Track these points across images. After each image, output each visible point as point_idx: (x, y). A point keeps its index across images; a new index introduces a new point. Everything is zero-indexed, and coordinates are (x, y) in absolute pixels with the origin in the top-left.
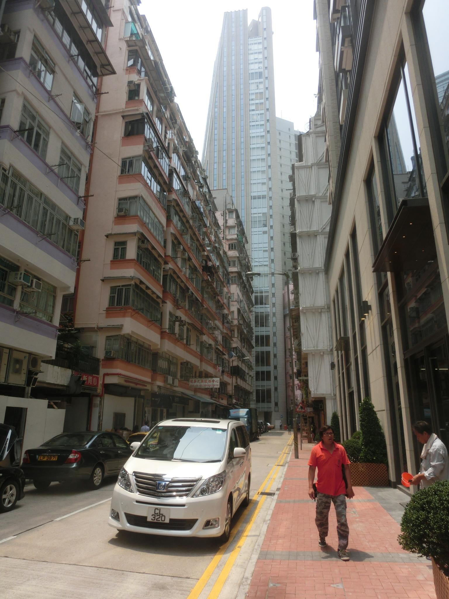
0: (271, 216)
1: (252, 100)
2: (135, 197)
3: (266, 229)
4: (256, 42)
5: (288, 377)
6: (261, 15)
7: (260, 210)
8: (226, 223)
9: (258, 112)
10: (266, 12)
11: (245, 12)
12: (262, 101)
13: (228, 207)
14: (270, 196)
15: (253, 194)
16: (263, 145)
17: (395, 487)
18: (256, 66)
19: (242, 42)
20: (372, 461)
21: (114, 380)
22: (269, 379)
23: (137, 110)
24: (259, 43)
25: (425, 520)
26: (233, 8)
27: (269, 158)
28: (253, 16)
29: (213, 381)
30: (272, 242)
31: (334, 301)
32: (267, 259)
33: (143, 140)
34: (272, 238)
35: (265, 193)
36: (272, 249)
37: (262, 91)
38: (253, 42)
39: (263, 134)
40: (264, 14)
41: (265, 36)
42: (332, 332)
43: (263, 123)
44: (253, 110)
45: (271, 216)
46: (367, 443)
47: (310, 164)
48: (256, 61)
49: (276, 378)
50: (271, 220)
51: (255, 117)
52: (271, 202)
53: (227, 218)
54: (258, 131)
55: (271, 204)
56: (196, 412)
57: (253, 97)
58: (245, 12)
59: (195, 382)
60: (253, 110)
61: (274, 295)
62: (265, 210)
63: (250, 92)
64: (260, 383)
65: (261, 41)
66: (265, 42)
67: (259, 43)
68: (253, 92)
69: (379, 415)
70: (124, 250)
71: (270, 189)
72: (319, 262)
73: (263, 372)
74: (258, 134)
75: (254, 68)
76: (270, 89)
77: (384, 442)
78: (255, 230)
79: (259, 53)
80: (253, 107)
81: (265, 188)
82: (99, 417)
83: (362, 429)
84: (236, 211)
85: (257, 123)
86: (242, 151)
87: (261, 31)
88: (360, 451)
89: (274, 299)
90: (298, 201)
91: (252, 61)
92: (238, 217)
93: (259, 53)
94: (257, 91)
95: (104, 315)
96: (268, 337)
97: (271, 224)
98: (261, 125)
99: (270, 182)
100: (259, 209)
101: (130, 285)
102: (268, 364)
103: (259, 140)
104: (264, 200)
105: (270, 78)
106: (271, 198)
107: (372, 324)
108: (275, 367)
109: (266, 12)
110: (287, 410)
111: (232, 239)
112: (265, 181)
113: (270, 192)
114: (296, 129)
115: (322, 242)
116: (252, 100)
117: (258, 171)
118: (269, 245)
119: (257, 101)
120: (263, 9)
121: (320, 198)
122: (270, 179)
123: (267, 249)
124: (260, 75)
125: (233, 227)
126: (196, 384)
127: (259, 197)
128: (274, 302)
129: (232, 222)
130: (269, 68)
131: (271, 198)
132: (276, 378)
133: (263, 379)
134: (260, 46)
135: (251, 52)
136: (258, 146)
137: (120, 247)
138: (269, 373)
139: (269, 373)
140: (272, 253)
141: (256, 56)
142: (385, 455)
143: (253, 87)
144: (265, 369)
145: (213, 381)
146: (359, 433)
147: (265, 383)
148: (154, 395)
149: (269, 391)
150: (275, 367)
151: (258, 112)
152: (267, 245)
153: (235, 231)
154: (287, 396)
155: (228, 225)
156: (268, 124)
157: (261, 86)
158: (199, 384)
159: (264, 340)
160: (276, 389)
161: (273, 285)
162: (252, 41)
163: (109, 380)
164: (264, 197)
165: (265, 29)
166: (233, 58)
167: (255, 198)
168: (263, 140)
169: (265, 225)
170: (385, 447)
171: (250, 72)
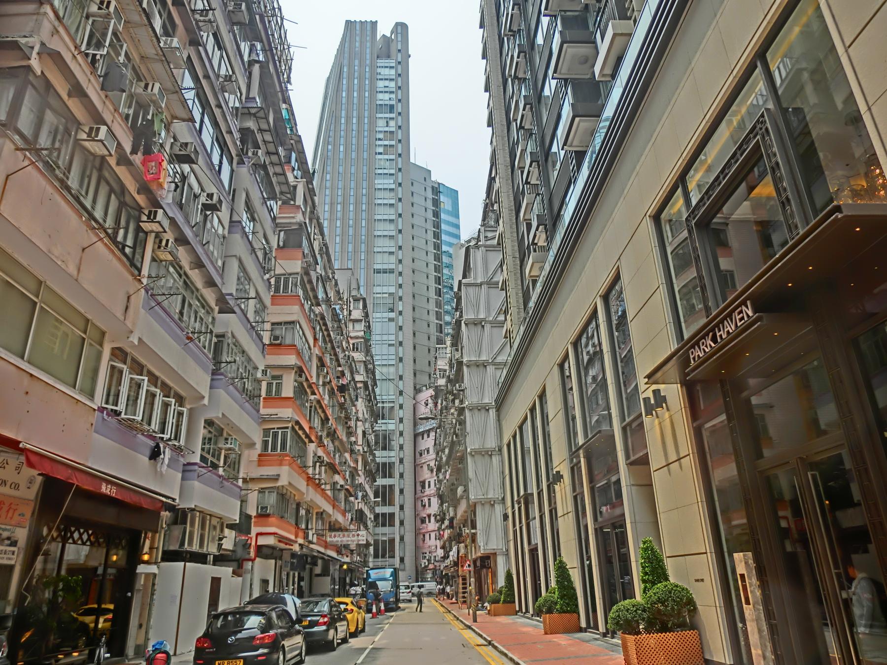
0: (400, 299)
1: (380, 139)
2: (293, 322)
3: (392, 315)
4: (386, 65)
5: (419, 521)
6: (394, 30)
7: (385, 289)
8: (350, 314)
9: (386, 157)
10: (401, 29)
11: (374, 24)
12: (393, 143)
13: (354, 293)
14: (400, 270)
15: (377, 267)
16: (393, 202)
17: (586, 632)
18: (387, 96)
19: (368, 62)
20: (564, 612)
21: (270, 541)
22: (392, 524)
23: (293, 217)
24: (391, 67)
25: (619, 616)
26: (358, 16)
27: (400, 220)
28: (384, 29)
29: (358, 535)
30: (400, 333)
31: (509, 445)
32: (393, 357)
33: (301, 254)
34: (401, 328)
35: (393, 266)
36: (401, 344)
37: (393, 129)
38: (381, 65)
39: (393, 186)
40: (399, 31)
41: (399, 60)
42: (504, 478)
43: (393, 171)
44: (380, 154)
45: (400, 299)
46: (562, 597)
47: (479, 281)
48: (387, 89)
49: (402, 523)
50: (400, 303)
51: (382, 163)
52: (400, 278)
53: (351, 308)
54: (386, 181)
55: (400, 282)
56: (324, 575)
57: (381, 136)
58: (374, 24)
59: (335, 536)
60: (380, 154)
61: (401, 407)
62: (392, 290)
63: (377, 129)
64: (380, 530)
65: (393, 65)
66: (399, 67)
67: (391, 67)
68: (380, 129)
69: (571, 572)
70: (279, 386)
71: (400, 261)
72: (489, 398)
73: (384, 515)
74: (386, 186)
75: (384, 98)
76: (404, 127)
77: (576, 594)
78: (379, 315)
79: (392, 80)
80: (381, 150)
81: (393, 259)
82: (251, 585)
83: (557, 584)
84: (364, 300)
85: (386, 171)
86: (364, 207)
87: (394, 47)
88: (556, 603)
89: (401, 411)
90: (466, 324)
91: (381, 90)
92: (365, 306)
93: (392, 80)
94: (387, 129)
95: (256, 463)
96: (391, 465)
97: (401, 309)
98: (391, 175)
99: (400, 252)
100: (385, 287)
101: (287, 428)
102: (391, 503)
103: (387, 194)
104: (391, 275)
105: (405, 115)
106: (400, 274)
107: (563, 491)
108: (402, 508)
109: (401, 29)
110: (416, 567)
111: (357, 338)
112: (393, 250)
113: (400, 266)
114: (433, 179)
115: (494, 377)
116: (380, 139)
117: (384, 236)
118: (397, 337)
119: (386, 143)
120: (397, 24)
121: (491, 322)
122: (400, 248)
123: (393, 342)
124: (391, 108)
125: (360, 321)
126: (336, 539)
127: (385, 271)
128: (401, 416)
129: (357, 314)
130: (404, 100)
131: (400, 274)
132: (402, 523)
133: (384, 525)
134: (393, 72)
135: (379, 77)
136: (385, 202)
137: (275, 382)
138: (392, 515)
139: (392, 515)
140: (401, 349)
141: (387, 83)
142: (577, 606)
143: (381, 123)
144: (386, 510)
145: (358, 535)
146: (554, 589)
147: (386, 530)
148: (293, 555)
149: (392, 541)
150: (402, 508)
151: (386, 157)
152: (393, 337)
153: (361, 326)
154: (417, 547)
155: (352, 317)
156: (400, 174)
157: (392, 123)
158: (339, 539)
159: (386, 470)
160: (402, 539)
161: (401, 393)
162: (381, 62)
163: (262, 541)
164: (391, 271)
165: (399, 51)
166: (356, 81)
167: (378, 271)
168: (392, 194)
169: (392, 310)
170: (576, 599)
171: (379, 102)
